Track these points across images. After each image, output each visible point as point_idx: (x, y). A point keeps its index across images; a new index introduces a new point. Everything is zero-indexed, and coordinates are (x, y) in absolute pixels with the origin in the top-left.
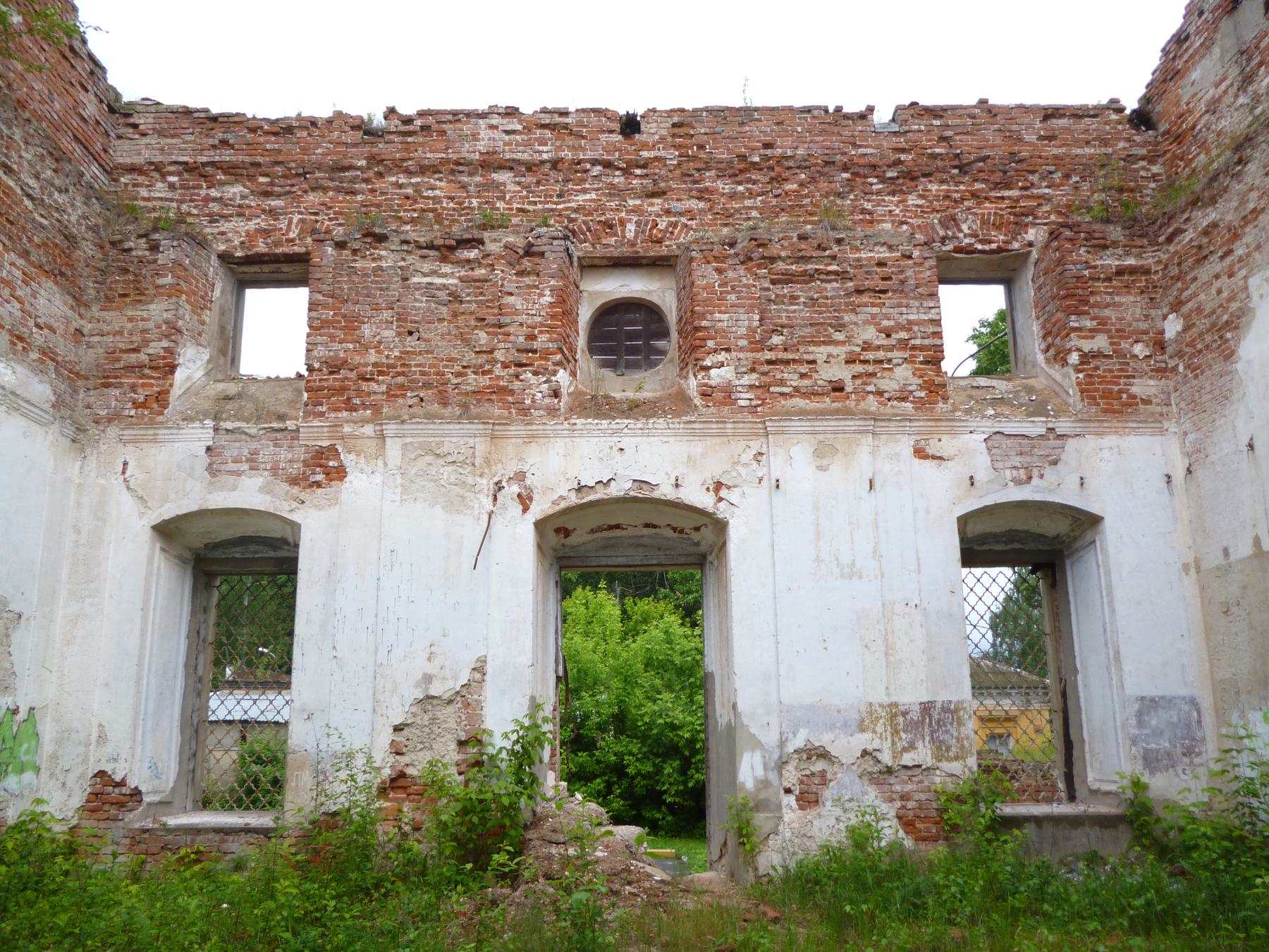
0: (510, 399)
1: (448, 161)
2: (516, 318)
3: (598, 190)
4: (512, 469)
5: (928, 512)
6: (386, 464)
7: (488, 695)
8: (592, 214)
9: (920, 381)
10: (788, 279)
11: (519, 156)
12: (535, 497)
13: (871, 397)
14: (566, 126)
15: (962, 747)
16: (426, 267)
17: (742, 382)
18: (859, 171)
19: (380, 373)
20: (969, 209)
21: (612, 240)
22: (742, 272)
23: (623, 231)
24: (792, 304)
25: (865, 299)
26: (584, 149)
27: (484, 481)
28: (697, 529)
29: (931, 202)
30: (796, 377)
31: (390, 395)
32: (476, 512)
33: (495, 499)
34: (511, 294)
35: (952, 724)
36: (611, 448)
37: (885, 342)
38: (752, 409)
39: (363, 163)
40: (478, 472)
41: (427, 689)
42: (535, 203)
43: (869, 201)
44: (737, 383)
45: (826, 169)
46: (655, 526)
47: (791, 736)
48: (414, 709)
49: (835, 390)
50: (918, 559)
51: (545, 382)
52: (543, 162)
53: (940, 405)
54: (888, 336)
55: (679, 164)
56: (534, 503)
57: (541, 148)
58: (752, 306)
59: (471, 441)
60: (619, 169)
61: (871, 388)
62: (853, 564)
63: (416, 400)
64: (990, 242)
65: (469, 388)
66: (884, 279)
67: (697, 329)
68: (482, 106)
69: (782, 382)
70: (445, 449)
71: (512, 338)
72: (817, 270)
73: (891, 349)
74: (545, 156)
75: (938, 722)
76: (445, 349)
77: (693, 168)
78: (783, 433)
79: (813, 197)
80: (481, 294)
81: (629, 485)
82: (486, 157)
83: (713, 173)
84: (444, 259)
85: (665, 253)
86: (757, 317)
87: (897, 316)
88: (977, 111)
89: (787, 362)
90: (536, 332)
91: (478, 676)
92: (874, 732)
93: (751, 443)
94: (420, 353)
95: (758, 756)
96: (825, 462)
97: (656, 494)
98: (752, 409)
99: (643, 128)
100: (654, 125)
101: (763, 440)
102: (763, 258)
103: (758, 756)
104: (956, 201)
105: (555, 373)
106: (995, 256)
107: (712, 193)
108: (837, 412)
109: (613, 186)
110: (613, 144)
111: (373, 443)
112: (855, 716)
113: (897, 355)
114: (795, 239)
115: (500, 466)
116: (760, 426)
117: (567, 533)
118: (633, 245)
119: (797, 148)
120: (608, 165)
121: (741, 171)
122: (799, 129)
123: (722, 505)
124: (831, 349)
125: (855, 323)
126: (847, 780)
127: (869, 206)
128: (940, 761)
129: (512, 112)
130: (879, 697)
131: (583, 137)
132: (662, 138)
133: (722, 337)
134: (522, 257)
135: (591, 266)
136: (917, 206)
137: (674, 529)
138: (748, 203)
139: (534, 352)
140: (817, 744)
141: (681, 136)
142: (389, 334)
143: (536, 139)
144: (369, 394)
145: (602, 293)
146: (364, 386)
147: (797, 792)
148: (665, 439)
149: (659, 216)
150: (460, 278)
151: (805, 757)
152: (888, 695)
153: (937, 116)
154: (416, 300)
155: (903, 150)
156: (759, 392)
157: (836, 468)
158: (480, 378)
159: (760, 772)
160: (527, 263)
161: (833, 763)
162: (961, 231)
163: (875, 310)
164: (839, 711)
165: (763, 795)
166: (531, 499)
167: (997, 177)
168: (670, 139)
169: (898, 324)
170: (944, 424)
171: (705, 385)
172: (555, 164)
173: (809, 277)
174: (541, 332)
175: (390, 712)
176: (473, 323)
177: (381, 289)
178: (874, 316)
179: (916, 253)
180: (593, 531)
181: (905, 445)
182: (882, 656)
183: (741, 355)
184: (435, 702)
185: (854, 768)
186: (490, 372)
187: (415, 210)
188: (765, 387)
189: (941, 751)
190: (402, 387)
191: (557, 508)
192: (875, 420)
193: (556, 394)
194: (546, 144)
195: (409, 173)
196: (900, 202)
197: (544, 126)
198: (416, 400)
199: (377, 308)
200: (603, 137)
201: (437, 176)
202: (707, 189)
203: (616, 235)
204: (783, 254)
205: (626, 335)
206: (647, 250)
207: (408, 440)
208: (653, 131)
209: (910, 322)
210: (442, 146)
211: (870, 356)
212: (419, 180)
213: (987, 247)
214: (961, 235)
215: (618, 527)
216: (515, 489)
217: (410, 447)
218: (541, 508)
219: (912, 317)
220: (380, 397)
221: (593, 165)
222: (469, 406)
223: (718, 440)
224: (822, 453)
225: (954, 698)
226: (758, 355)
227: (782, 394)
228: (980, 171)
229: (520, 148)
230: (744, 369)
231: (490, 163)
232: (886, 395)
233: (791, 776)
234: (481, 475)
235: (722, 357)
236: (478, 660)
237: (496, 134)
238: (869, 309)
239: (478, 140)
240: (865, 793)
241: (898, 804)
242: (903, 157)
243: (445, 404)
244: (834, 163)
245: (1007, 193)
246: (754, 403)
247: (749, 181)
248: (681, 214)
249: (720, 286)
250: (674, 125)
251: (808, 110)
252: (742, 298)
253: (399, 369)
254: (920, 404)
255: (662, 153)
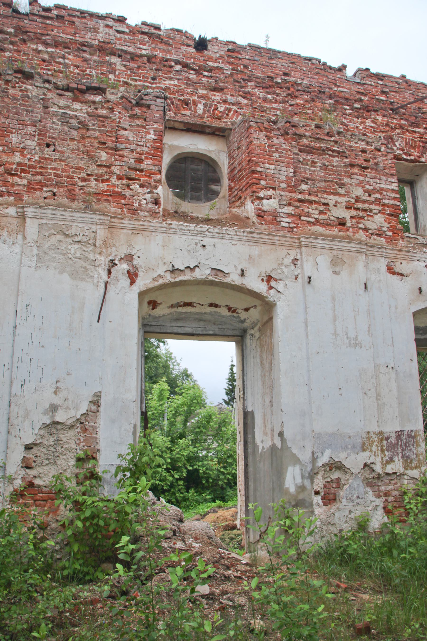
0: (123, 201)
1: (75, 42)
2: (129, 146)
3: (179, 79)
4: (123, 251)
5: (396, 308)
6: (24, 238)
7: (102, 423)
8: (175, 94)
9: (388, 226)
10: (309, 150)
11: (126, 48)
12: (140, 274)
13: (361, 231)
14: (158, 36)
15: (419, 460)
16: (62, 102)
17: (283, 211)
18: (340, 101)
19: (23, 171)
20: (399, 134)
21: (188, 113)
22: (282, 141)
23: (195, 108)
24: (312, 166)
25: (356, 170)
26: (170, 53)
27: (102, 258)
28: (247, 310)
29: (379, 126)
30: (317, 212)
31: (31, 187)
32: (96, 281)
33: (110, 273)
34: (125, 129)
35: (413, 445)
36: (196, 244)
37: (368, 199)
38: (291, 230)
39: (11, 30)
40: (98, 251)
41: (53, 416)
42: (136, 80)
43: (345, 118)
44: (281, 211)
45: (320, 96)
46: (216, 306)
47: (320, 454)
48: (42, 432)
49: (340, 224)
50: (392, 338)
51: (149, 193)
52: (142, 56)
53: (401, 241)
54: (370, 195)
55: (232, 74)
56: (139, 278)
57: (141, 46)
58: (289, 163)
59: (93, 228)
60: (193, 69)
61: (361, 226)
62: (356, 338)
63: (49, 194)
64: (410, 155)
65: (92, 190)
66: (365, 161)
67: (254, 172)
68: (102, 11)
69: (308, 215)
70: (73, 231)
71: (125, 159)
72: (327, 148)
73: (371, 203)
74: (144, 52)
75: (405, 444)
76: (74, 160)
77: (241, 80)
78: (312, 247)
79: (313, 110)
80: (103, 126)
81: (208, 272)
82: (103, 45)
83: (253, 84)
84: (75, 99)
85: (223, 126)
86: (292, 171)
87: (374, 184)
88: (401, 81)
89: (311, 202)
90: (143, 157)
91: (94, 408)
92: (371, 451)
93: (290, 252)
94: (55, 160)
95: (297, 468)
96: (337, 269)
97: (227, 280)
98: (291, 230)
99: (209, 47)
100: (217, 47)
101: (298, 250)
102: (295, 134)
103: (297, 468)
104: (392, 128)
105: (156, 187)
106: (412, 164)
107: (252, 95)
108: (343, 237)
109: (188, 79)
110: (190, 53)
111: (15, 221)
112: (359, 441)
113: (376, 208)
114: (313, 127)
115: (114, 249)
116: (296, 241)
117: (154, 304)
118: (202, 118)
119: (303, 79)
120: (185, 66)
121: (270, 87)
122: (305, 69)
123: (272, 292)
124: (336, 198)
125: (351, 184)
126: (355, 484)
127: (345, 121)
128: (407, 469)
129: (121, 20)
130: (374, 428)
131: (172, 46)
132: (221, 57)
133: (270, 180)
134: (134, 106)
135: (172, 127)
136: (371, 127)
137: (230, 309)
138: (275, 106)
139: (141, 171)
140: (337, 460)
141: (233, 58)
142: (31, 143)
143: (139, 40)
144: (13, 185)
145: (178, 147)
146: (10, 179)
147: (322, 494)
148: (234, 242)
149: (219, 103)
150: (88, 113)
151: (328, 469)
152: (378, 426)
153: (379, 79)
154: (53, 123)
155: (362, 94)
156: (294, 219)
157: (344, 274)
158: (101, 185)
159: (299, 481)
160: (137, 110)
161: (346, 473)
162: (395, 146)
163: (362, 178)
164: (350, 437)
165: (301, 497)
166: (136, 275)
167: (413, 119)
168: (226, 58)
169: (375, 189)
170: (404, 253)
171: (260, 209)
172: (150, 59)
173: (323, 151)
174: (147, 158)
175: (22, 434)
176: (96, 145)
177: (27, 111)
178: (361, 182)
179: (383, 149)
180: (172, 306)
181: (382, 264)
182: (375, 400)
183: (282, 193)
184: (59, 427)
185: (360, 475)
186: (108, 181)
187: (49, 70)
188: (299, 216)
189: (408, 463)
190: (39, 183)
191: (156, 284)
192: (367, 246)
193: (156, 202)
194: (145, 45)
195: (46, 44)
196: (362, 123)
197: (143, 33)
198: (49, 194)
199: (23, 123)
200: (184, 48)
201: (66, 50)
202: (249, 93)
203: (190, 110)
204: (307, 134)
205: (192, 178)
206: (211, 122)
207: (44, 221)
208: (216, 51)
209: (382, 189)
210: (72, 31)
211: (360, 206)
212: (53, 50)
213: (409, 158)
214: (395, 148)
215: (190, 304)
216: (125, 266)
217: (45, 227)
218: (144, 282)
219: (382, 186)
220: (21, 188)
221: (176, 64)
222: (91, 202)
223: (269, 247)
224: (336, 263)
225: (414, 429)
226: (294, 195)
227: (308, 222)
228: (404, 114)
229: (127, 44)
230: (285, 203)
231: (104, 49)
232: (370, 231)
233: (319, 483)
234: (100, 254)
235: (270, 192)
236: (95, 395)
237: (112, 32)
238: (358, 177)
239: (98, 33)
240: (366, 493)
241: (383, 499)
242: (363, 98)
243: (73, 199)
244: (324, 93)
245: (417, 130)
246: (291, 225)
247: (274, 93)
248: (233, 104)
249: (268, 146)
250: (229, 50)
251: (309, 59)
252: (283, 157)
253: (38, 170)
254: (389, 239)
255: (221, 65)
